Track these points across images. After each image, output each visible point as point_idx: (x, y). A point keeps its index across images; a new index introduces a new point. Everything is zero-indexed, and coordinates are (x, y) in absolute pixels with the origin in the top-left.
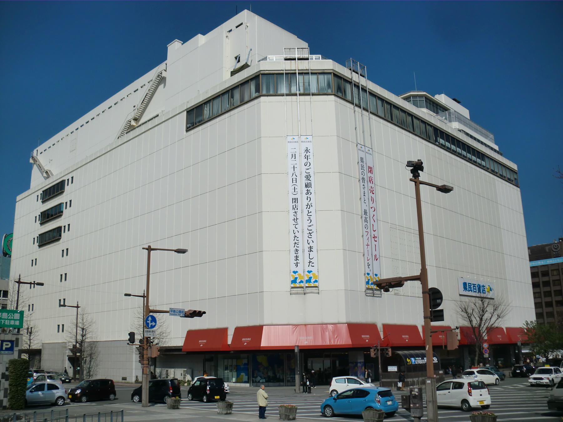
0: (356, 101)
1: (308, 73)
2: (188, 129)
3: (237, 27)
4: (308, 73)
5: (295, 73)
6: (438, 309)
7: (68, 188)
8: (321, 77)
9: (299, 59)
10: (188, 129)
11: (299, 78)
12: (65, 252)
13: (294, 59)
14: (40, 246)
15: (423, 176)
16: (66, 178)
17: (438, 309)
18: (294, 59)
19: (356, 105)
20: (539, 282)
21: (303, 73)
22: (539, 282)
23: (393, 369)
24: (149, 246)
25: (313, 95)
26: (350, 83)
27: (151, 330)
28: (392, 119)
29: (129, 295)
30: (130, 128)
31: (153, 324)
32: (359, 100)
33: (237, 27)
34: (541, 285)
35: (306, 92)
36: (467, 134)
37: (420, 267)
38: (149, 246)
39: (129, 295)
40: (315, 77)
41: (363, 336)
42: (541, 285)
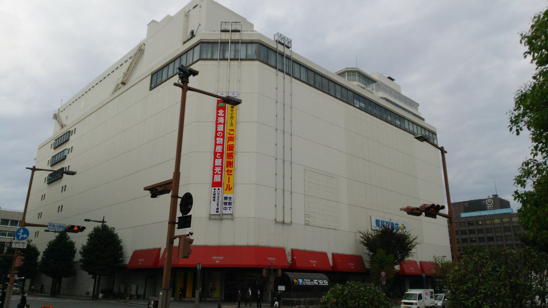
0: (279, 66)
1: (238, 43)
2: (151, 89)
3: (194, 8)
4: (238, 43)
5: (228, 42)
6: (188, 215)
7: (72, 138)
8: (250, 46)
9: (233, 31)
10: (151, 89)
11: (230, 47)
12: (64, 188)
13: (228, 31)
14: (48, 184)
15: (193, 81)
16: (70, 130)
17: (188, 215)
18: (228, 31)
19: (279, 70)
20: (478, 233)
21: (235, 43)
22: (478, 233)
23: (282, 288)
24: (34, 167)
25: (241, 60)
26: (276, 52)
27: (21, 241)
28: (315, 83)
29: (89, 220)
30: (117, 88)
31: (25, 236)
32: (283, 64)
33: (194, 8)
34: (486, 239)
35: (236, 57)
36: (387, 100)
37: (173, 170)
38: (34, 167)
39: (89, 220)
40: (244, 46)
41: (213, 258)
42: (486, 239)
